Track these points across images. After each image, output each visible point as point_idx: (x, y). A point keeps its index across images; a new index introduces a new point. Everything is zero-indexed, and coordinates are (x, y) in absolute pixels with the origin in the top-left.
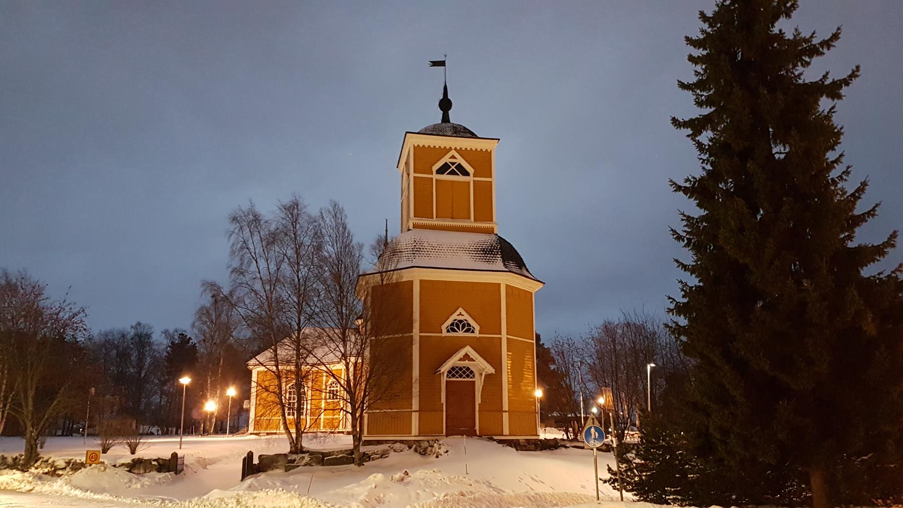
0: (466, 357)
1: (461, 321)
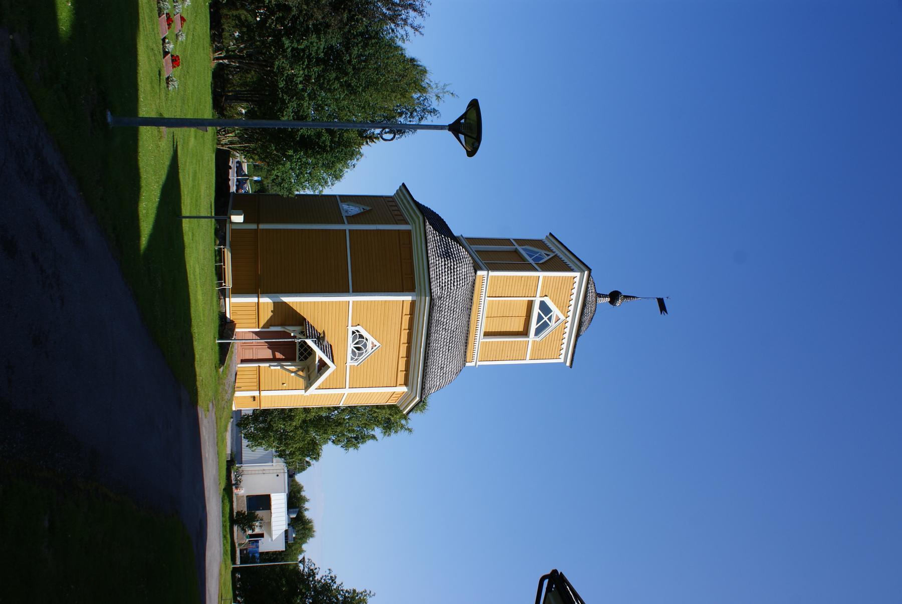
1: (365, 346)
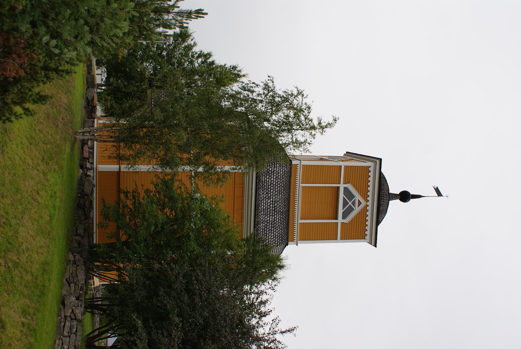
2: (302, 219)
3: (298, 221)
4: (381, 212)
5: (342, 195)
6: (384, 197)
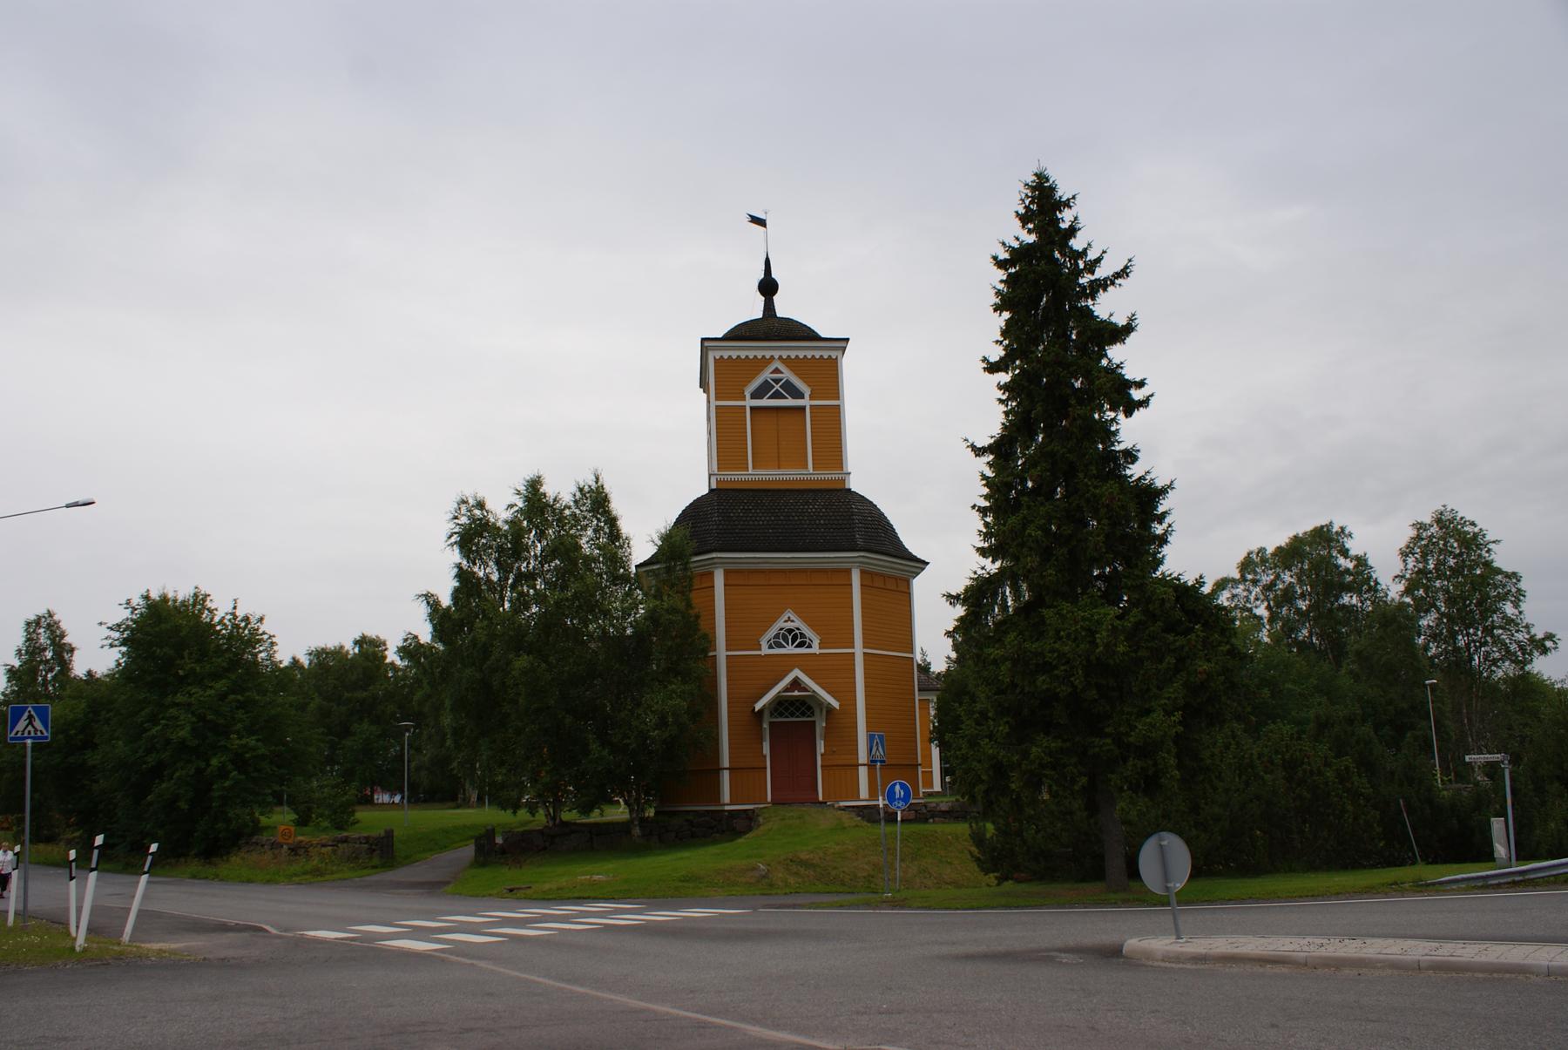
0: (796, 684)
2: (806, 467)
3: (808, 473)
4: (798, 332)
5: (765, 402)
6: (771, 328)
